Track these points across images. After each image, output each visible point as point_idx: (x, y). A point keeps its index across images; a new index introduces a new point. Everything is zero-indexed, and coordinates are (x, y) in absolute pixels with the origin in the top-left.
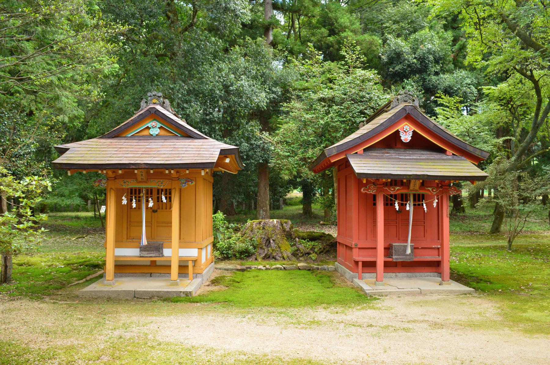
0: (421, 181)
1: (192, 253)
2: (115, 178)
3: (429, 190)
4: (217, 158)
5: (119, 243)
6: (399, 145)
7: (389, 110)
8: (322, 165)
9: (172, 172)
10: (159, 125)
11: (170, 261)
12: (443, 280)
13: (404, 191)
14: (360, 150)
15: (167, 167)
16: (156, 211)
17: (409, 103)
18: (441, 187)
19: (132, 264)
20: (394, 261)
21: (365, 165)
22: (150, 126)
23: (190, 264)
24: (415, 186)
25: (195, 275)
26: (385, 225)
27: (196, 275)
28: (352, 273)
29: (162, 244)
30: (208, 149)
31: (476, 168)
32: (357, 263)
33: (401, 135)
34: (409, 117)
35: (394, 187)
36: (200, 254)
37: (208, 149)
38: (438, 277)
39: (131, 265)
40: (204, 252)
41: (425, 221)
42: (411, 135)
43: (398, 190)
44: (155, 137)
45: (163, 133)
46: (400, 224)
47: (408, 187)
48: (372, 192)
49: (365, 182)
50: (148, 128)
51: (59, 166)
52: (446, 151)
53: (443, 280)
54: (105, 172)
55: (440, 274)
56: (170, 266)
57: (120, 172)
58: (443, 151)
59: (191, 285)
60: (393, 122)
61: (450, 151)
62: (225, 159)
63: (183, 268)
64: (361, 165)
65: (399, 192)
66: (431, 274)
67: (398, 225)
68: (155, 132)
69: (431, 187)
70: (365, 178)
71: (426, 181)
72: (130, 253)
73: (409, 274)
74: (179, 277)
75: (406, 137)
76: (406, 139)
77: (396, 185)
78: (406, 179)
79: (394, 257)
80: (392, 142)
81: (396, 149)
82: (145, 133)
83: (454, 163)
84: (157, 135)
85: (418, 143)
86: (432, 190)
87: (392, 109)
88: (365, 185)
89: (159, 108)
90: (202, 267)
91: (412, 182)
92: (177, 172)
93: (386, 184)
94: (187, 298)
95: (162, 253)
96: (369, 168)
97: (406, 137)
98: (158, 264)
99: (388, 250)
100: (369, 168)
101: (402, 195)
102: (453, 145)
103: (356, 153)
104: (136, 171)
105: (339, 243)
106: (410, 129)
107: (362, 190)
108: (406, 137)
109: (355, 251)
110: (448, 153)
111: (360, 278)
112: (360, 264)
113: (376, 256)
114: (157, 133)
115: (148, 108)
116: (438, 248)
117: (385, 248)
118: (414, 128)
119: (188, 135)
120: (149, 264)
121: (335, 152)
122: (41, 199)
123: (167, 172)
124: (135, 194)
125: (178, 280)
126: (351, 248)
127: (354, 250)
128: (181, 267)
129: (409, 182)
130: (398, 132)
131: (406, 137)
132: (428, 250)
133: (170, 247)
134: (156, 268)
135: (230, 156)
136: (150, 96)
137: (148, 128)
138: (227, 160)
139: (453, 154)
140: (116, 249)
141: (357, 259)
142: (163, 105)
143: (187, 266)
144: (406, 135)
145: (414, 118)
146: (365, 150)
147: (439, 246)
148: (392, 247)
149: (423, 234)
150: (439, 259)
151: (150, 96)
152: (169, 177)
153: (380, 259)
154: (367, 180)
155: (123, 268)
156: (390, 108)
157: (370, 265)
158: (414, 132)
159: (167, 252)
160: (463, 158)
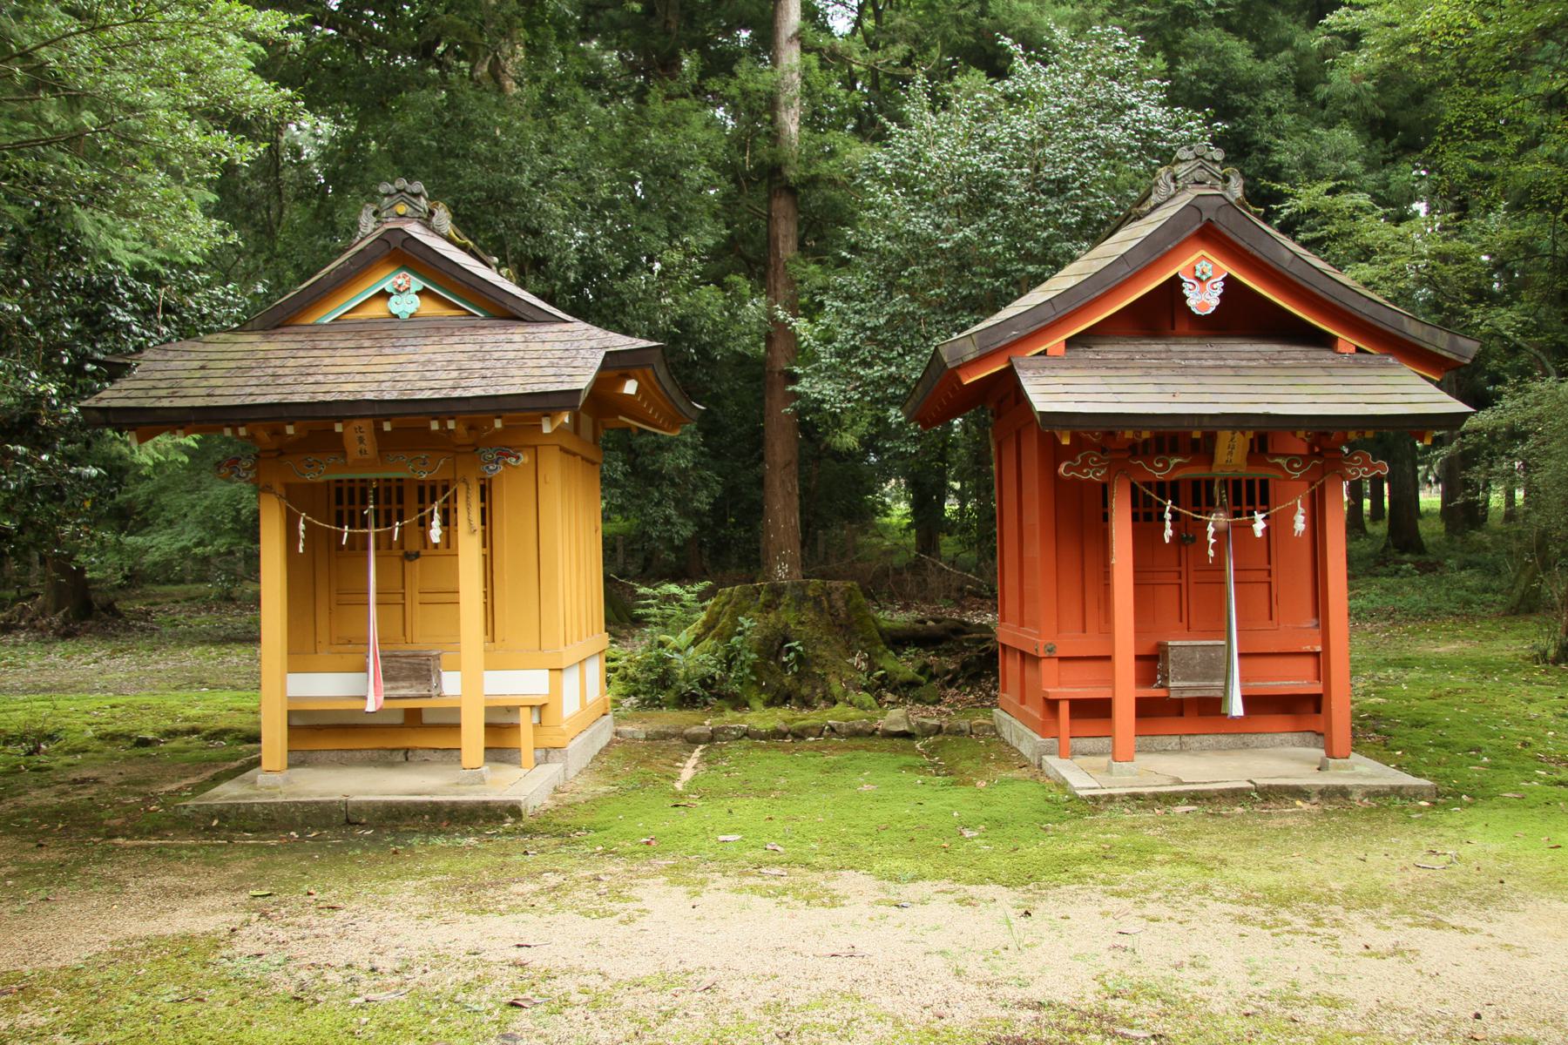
0: (1250, 434)
1: (519, 684)
2: (281, 452)
3: (1278, 466)
4: (590, 378)
5: (301, 655)
6: (1182, 326)
7: (1147, 214)
8: (941, 395)
9: (451, 425)
10: (417, 284)
11: (457, 711)
12: (1330, 755)
13: (1198, 472)
14: (1055, 343)
15: (437, 408)
16: (417, 555)
17: (1212, 187)
18: (1319, 455)
19: (345, 721)
20: (1173, 695)
21: (1068, 389)
22: (388, 290)
23: (526, 720)
24: (1231, 455)
25: (539, 753)
26: (1138, 584)
27: (547, 754)
28: (1039, 739)
29: (438, 657)
30: (563, 355)
31: (1432, 388)
32: (1052, 705)
33: (1186, 292)
34: (1211, 236)
35: (1171, 465)
36: (556, 688)
37: (563, 355)
38: (1316, 746)
39: (355, 727)
40: (570, 681)
41: (1273, 567)
42: (1220, 291)
43: (1178, 466)
44: (405, 321)
45: (431, 309)
46: (1191, 581)
47: (1209, 458)
48: (1094, 475)
49: (1066, 442)
50: (384, 295)
51: (95, 414)
52: (1335, 338)
53: (1330, 755)
54: (242, 431)
55: (1323, 736)
56: (457, 727)
57: (290, 430)
58: (1327, 342)
59: (522, 785)
60: (1157, 250)
61: (1347, 342)
62: (623, 383)
63: (501, 732)
64: (1054, 390)
65: (1179, 475)
66: (1278, 738)
67: (1183, 581)
68: (407, 304)
69: (1284, 456)
70: (1065, 427)
71: (1265, 433)
72: (325, 687)
73: (1224, 739)
74: (487, 760)
75: (1204, 297)
76: (1204, 305)
77: (1175, 452)
78: (1199, 427)
79: (1171, 684)
80: (1161, 316)
81: (1173, 340)
82: (377, 310)
83: (1358, 376)
84: (412, 316)
85: (1242, 318)
86: (1290, 465)
87: (1153, 209)
88: (1069, 453)
89: (415, 230)
90: (564, 727)
91: (1224, 437)
92: (471, 428)
93: (1137, 449)
94: (556, 828)
95: (439, 685)
96: (1083, 398)
97: (1204, 297)
98: (427, 719)
99: (1151, 663)
100: (1083, 398)
101: (1196, 483)
102: (1356, 318)
103: (1044, 353)
104: (339, 428)
105: (1004, 646)
106: (1216, 268)
107: (1061, 470)
108: (1203, 299)
109: (1048, 668)
110: (1341, 347)
111: (1066, 753)
112: (1064, 708)
113: (1110, 682)
114: (412, 310)
115: (381, 230)
116: (1317, 654)
117: (1138, 658)
118: (1227, 269)
119: (504, 312)
120: (399, 720)
121: (971, 353)
122: (881, 615)
123: (435, 426)
124: (352, 502)
125: (485, 768)
126: (1036, 660)
127: (1044, 664)
128: (491, 728)
129: (1210, 438)
130: (1175, 283)
131: (1203, 299)
132: (1282, 661)
133: (456, 667)
134: (414, 731)
135: (637, 371)
136: (389, 195)
137: (384, 295)
138: (630, 387)
139: (1359, 350)
140: (291, 677)
141: (1053, 692)
142: (427, 221)
143: (515, 727)
144: (1202, 291)
145: (1228, 234)
146: (1070, 343)
147: (1318, 649)
148: (1166, 652)
149: (1266, 611)
150: (1317, 688)
151: (389, 195)
152: (443, 443)
153: (1125, 691)
154: (1074, 437)
155: (317, 732)
156: (1145, 208)
157: (1094, 711)
158: (1229, 281)
159: (451, 684)
160: (1391, 360)
